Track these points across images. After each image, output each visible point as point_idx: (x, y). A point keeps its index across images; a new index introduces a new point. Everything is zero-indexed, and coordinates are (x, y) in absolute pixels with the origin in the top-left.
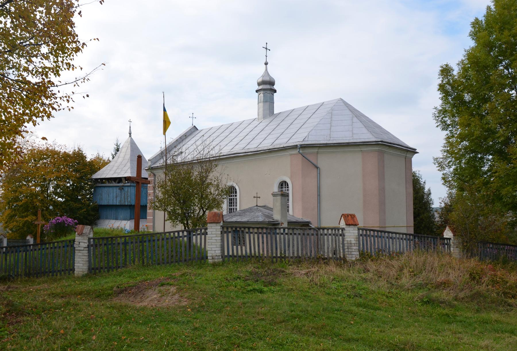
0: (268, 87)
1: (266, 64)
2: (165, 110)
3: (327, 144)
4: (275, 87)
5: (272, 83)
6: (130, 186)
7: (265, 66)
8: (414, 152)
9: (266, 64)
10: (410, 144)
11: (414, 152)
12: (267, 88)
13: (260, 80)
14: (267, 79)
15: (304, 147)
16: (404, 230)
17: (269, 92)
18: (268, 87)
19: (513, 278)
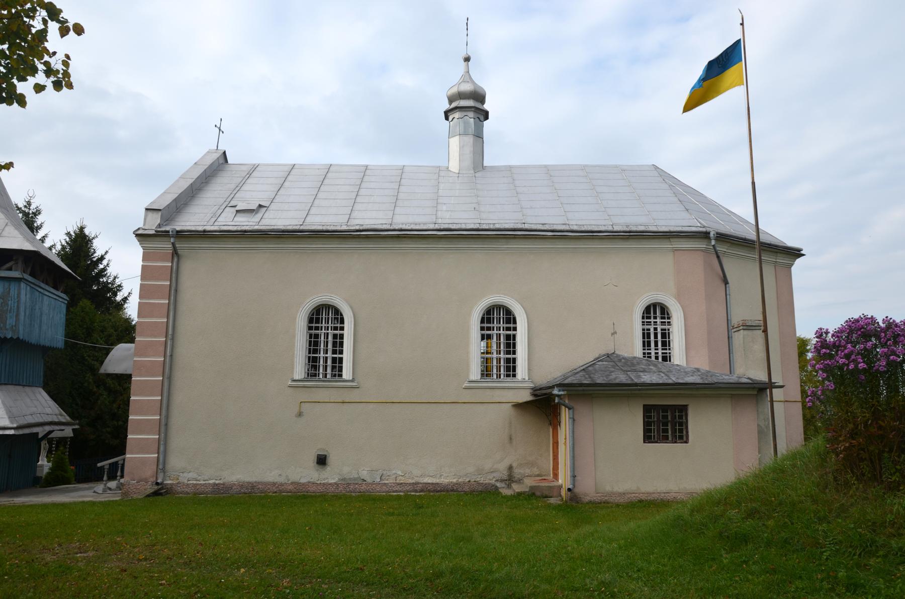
0: (470, 103)
1: (467, 59)
2: (753, 183)
3: (670, 232)
4: (486, 106)
5: (479, 97)
6: (19, 280)
7: (463, 64)
8: (796, 253)
9: (467, 59)
10: (791, 242)
11: (796, 253)
12: (470, 106)
13: (455, 90)
14: (467, 87)
15: (722, 238)
16: (175, 462)
17: (471, 114)
18: (470, 103)
19: (904, 503)
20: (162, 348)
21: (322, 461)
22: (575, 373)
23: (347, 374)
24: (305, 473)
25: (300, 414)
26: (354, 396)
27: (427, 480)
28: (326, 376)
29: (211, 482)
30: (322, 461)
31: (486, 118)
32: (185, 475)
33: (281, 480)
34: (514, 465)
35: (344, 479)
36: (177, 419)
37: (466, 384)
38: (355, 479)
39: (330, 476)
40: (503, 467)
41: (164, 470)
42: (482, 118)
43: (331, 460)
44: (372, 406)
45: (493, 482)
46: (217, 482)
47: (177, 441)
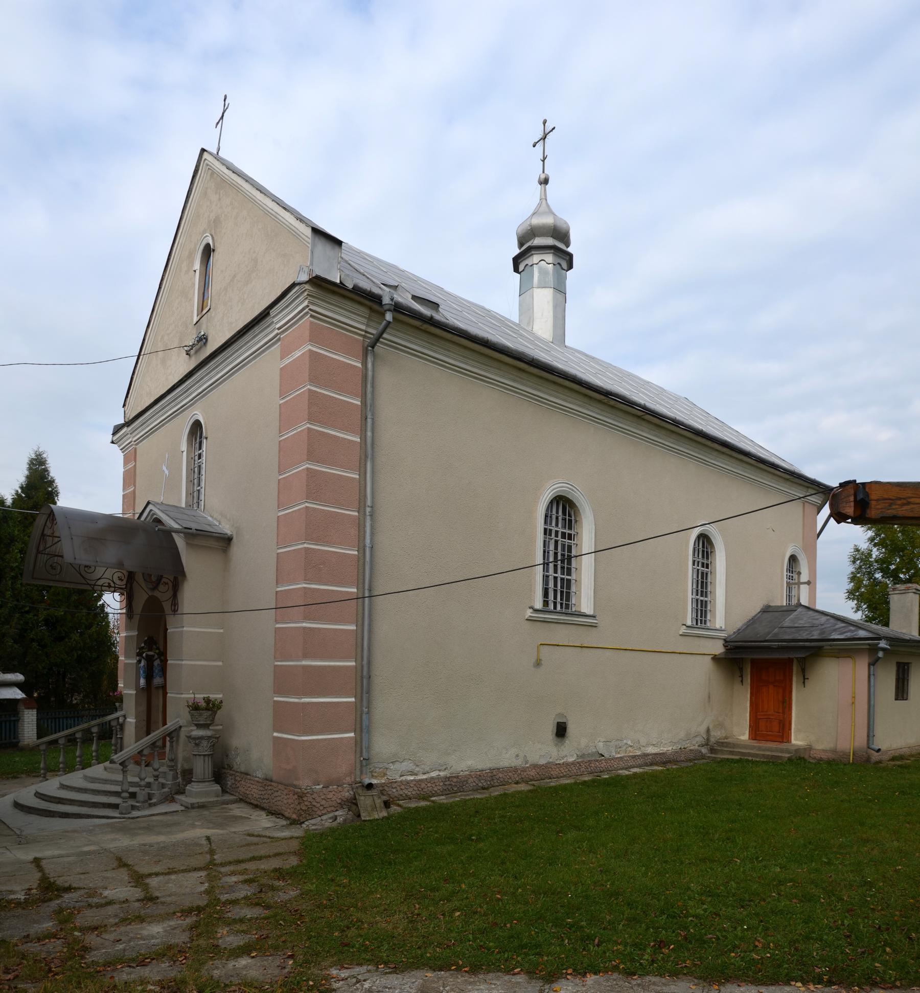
0: (550, 241)
1: (545, 182)
5: (562, 235)
16: (383, 745)
17: (549, 258)
20: (354, 532)
21: (561, 731)
22: (752, 622)
23: (585, 601)
24: (542, 751)
25: (538, 664)
26: (590, 638)
27: (651, 750)
28: (555, 608)
29: (434, 774)
30: (561, 731)
31: (570, 266)
32: (397, 765)
33: (518, 763)
34: (711, 727)
35: (583, 756)
36: (383, 669)
37: (683, 630)
38: (593, 754)
39: (568, 753)
40: (702, 729)
41: (367, 761)
42: (565, 265)
43: (571, 729)
44: (608, 653)
45: (696, 747)
46: (442, 774)
47: (385, 705)
